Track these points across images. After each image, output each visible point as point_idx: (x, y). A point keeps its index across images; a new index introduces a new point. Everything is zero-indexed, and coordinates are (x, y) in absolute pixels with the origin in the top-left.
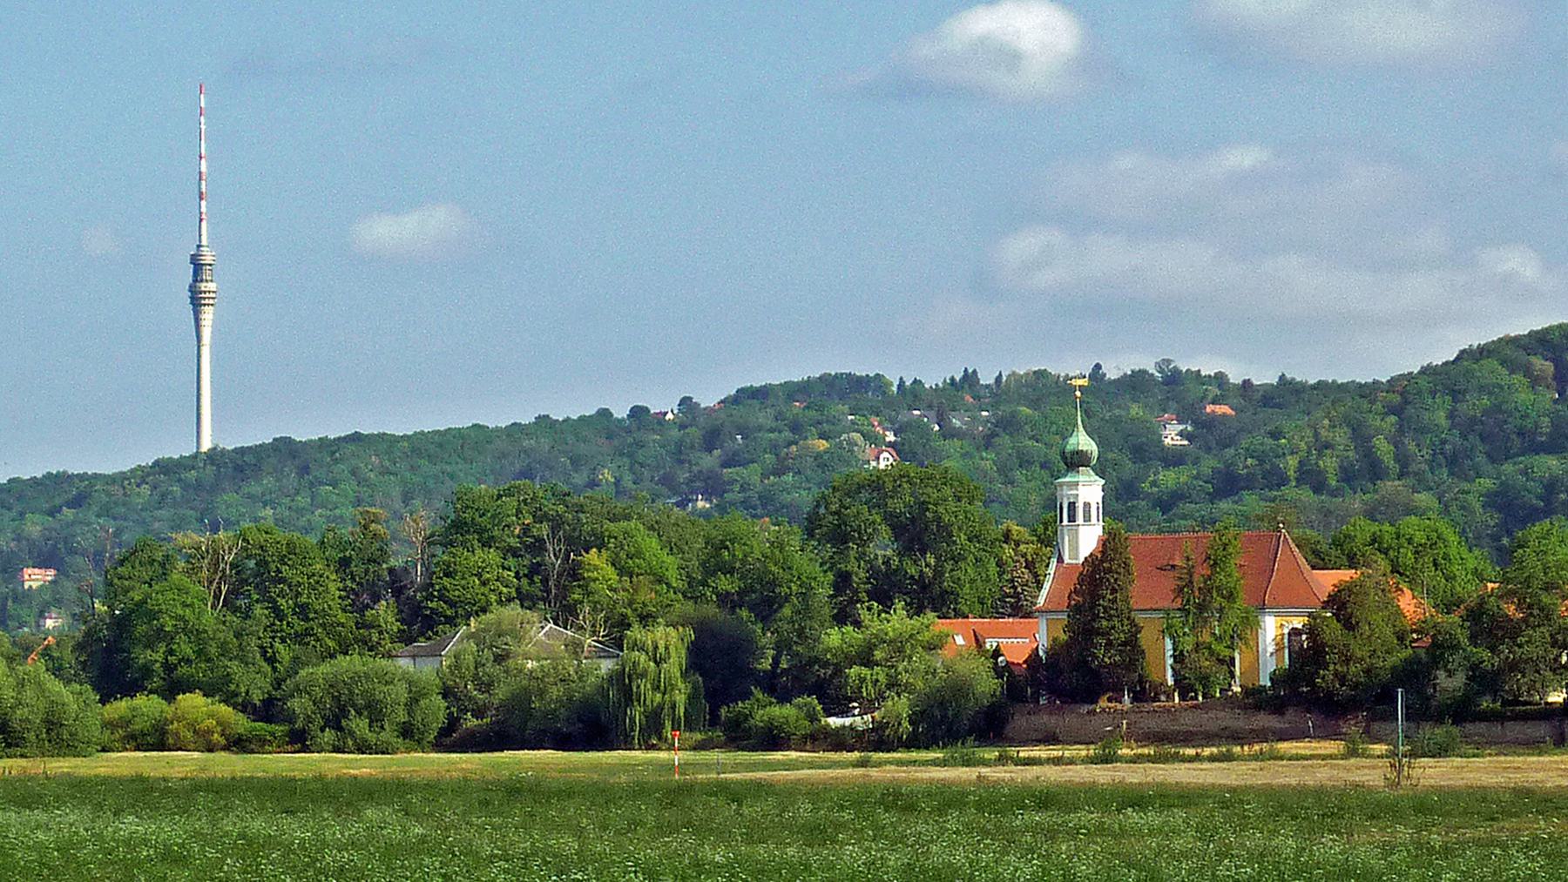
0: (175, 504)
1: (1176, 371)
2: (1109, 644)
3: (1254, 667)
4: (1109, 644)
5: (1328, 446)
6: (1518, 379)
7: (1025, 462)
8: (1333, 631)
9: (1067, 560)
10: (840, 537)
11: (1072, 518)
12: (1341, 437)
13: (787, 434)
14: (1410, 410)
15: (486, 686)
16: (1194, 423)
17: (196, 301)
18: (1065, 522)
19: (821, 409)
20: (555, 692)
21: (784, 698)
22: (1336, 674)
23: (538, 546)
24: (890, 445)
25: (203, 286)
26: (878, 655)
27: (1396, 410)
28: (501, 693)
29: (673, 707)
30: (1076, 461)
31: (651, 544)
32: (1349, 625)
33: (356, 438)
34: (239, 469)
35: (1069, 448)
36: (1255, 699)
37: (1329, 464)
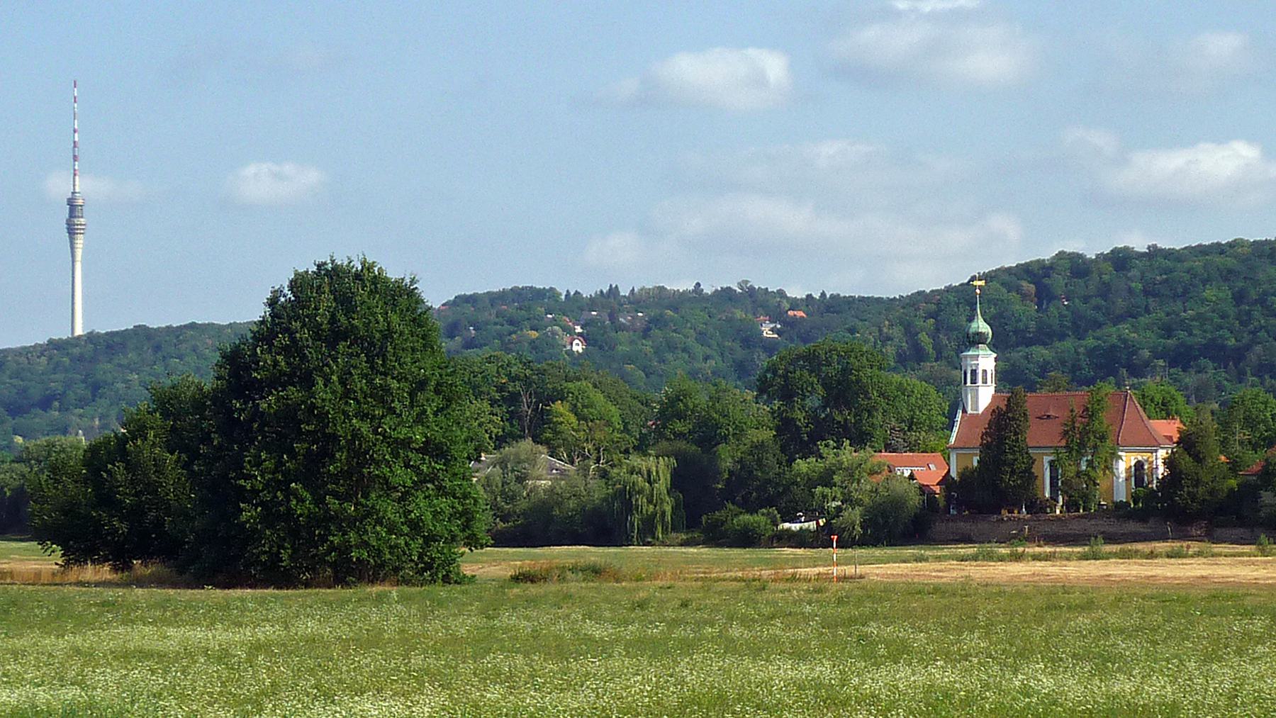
0: (66, 371)
1: (752, 288)
2: (1013, 472)
3: (1111, 490)
4: (1013, 472)
5: (889, 339)
6: (1014, 295)
7: (672, 347)
8: (1186, 462)
9: (969, 411)
10: (788, 394)
11: (974, 381)
12: (897, 332)
13: (507, 327)
14: (943, 315)
15: (511, 498)
16: (783, 323)
17: (72, 231)
18: (969, 384)
19: (529, 309)
20: (572, 504)
21: (752, 511)
22: (1189, 493)
23: (514, 399)
24: (579, 334)
25: (76, 221)
26: (836, 478)
27: (931, 315)
28: (523, 505)
29: (663, 513)
30: (977, 340)
31: (599, 398)
32: (1198, 459)
33: (193, 326)
34: (109, 347)
35: (972, 331)
36: (1119, 511)
37: (890, 350)
